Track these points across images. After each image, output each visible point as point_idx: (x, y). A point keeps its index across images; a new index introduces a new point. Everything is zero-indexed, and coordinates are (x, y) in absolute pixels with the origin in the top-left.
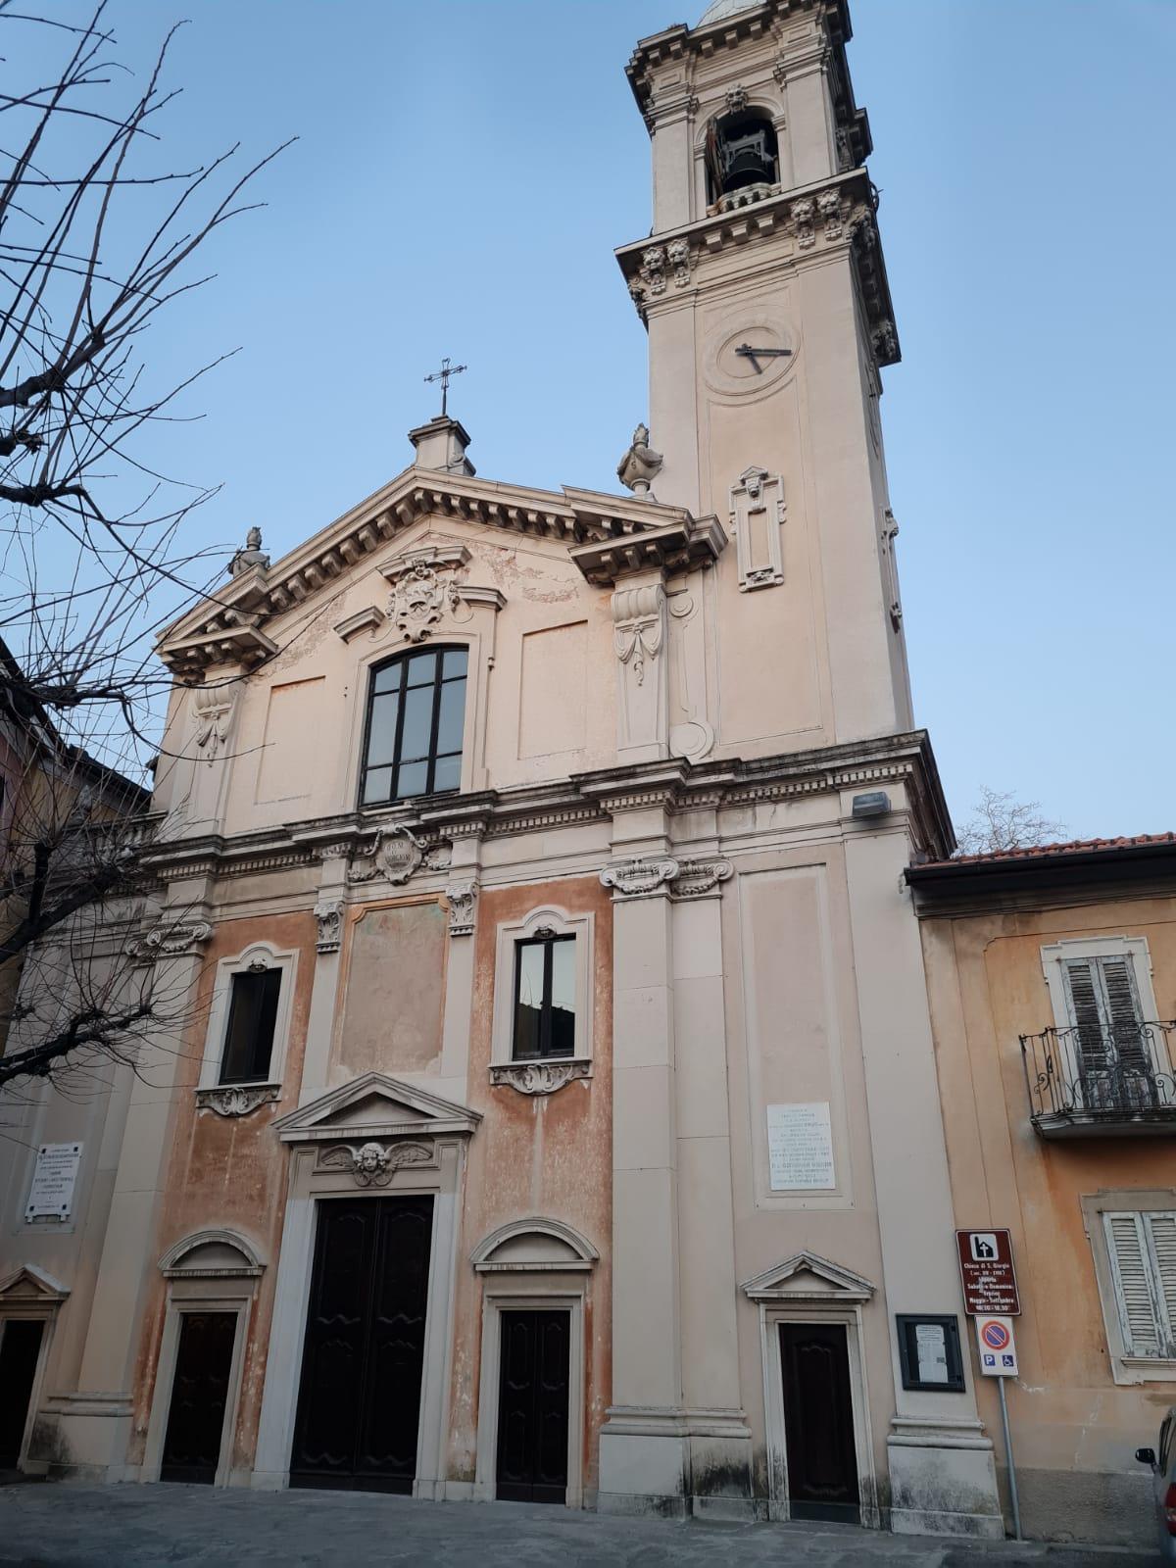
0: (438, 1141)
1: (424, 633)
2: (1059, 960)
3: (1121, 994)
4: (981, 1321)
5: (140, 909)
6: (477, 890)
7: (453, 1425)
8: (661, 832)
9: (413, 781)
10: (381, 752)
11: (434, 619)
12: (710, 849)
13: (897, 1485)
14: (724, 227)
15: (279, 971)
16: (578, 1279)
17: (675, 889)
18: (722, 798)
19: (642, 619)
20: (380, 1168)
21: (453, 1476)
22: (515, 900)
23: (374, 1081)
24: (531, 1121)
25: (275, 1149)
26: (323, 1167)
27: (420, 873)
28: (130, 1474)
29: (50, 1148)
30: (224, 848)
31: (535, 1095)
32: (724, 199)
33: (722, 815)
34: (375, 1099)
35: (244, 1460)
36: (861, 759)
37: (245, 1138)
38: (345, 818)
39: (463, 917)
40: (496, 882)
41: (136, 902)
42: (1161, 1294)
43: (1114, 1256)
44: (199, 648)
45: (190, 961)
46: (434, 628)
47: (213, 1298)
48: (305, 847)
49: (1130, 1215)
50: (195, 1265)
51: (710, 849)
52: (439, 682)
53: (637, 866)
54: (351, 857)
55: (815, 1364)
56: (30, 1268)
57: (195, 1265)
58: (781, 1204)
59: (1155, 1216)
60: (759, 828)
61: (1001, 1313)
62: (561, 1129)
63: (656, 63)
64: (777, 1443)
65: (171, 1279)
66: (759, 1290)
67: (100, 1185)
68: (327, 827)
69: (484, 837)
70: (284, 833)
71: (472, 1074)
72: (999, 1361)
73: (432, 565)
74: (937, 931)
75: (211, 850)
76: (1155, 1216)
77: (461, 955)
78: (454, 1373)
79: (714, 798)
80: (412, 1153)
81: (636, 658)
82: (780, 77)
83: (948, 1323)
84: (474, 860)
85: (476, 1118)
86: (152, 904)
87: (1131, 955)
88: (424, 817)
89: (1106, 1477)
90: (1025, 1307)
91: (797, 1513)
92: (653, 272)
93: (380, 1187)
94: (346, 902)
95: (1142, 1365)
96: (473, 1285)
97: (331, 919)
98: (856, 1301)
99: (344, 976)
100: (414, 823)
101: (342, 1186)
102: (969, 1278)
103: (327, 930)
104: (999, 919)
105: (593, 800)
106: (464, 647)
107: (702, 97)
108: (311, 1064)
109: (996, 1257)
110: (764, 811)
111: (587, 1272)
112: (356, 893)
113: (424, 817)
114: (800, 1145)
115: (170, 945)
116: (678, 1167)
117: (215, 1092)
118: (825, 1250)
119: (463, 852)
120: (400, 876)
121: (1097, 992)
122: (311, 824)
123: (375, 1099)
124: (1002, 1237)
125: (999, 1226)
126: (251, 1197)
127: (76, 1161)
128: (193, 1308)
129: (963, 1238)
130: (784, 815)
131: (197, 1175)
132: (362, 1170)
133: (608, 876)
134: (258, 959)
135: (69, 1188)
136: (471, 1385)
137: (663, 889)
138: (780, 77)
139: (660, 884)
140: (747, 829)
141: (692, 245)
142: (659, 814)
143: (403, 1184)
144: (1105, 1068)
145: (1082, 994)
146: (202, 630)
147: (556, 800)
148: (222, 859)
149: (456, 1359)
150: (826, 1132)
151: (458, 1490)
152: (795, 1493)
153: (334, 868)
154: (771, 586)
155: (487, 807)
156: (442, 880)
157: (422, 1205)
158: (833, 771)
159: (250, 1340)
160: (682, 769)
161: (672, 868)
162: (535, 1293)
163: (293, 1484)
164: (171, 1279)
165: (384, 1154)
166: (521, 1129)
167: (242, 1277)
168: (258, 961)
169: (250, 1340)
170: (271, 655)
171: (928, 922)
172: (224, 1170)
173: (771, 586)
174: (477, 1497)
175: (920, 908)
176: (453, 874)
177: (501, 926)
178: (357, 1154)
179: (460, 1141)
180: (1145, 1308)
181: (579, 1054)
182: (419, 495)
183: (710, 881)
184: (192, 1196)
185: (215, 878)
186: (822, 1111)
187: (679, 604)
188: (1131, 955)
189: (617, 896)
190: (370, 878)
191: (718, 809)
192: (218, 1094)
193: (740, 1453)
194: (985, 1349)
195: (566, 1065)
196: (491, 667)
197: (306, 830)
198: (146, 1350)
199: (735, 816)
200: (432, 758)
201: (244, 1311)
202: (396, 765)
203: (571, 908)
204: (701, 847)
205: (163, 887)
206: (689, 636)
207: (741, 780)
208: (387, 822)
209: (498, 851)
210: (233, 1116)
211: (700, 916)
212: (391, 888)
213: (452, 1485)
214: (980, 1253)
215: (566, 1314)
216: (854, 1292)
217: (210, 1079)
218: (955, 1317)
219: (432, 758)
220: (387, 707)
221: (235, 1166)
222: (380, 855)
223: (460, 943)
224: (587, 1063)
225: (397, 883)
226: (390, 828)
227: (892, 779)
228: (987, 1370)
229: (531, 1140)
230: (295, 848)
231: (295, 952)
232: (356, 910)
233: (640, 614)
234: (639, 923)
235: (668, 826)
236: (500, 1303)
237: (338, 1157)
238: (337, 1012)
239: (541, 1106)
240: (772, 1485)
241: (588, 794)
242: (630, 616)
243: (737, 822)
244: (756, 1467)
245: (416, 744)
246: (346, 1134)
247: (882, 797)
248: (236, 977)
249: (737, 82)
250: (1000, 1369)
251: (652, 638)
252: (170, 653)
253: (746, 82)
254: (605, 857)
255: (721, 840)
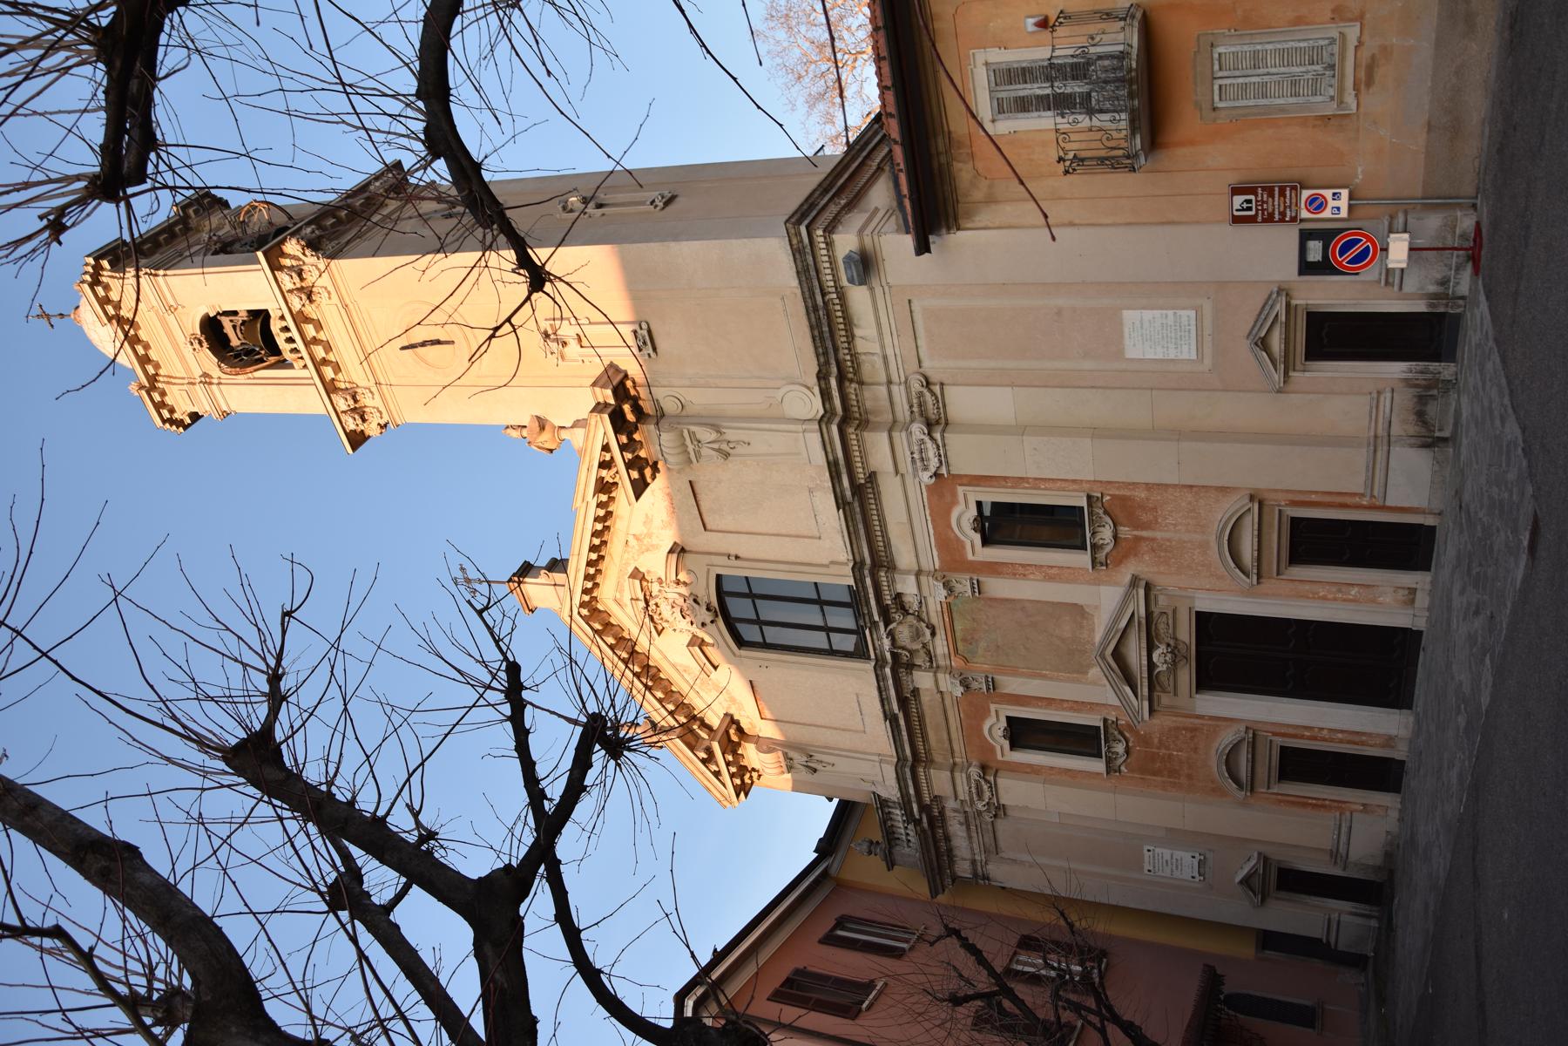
0: (1153, 608)
1: (708, 609)
2: (993, 121)
3: (1023, 74)
4: (1305, 214)
5: (955, 811)
6: (939, 575)
7: (1373, 601)
8: (885, 435)
9: (844, 619)
10: (818, 639)
11: (695, 601)
12: (899, 393)
13: (1432, 288)
14: (319, 365)
15: (1008, 718)
16: (1266, 509)
17: (935, 423)
18: (851, 381)
19: (688, 441)
20: (1174, 651)
21: (1412, 601)
22: (948, 545)
23: (1102, 656)
24: (1138, 539)
25: (1156, 721)
26: (1171, 689)
27: (924, 616)
28: (1394, 815)
29: (1147, 867)
30: (906, 759)
31: (1115, 537)
32: (288, 356)
33: (866, 378)
34: (1118, 655)
35: (1389, 741)
36: (813, 273)
37: (1145, 740)
38: (880, 678)
39: (963, 586)
40: (931, 559)
41: (949, 813)
42: (1283, 70)
43: (1252, 103)
44: (732, 776)
45: (1000, 781)
46: (703, 600)
47: (1268, 761)
48: (903, 702)
49: (1216, 88)
50: (1243, 772)
51: (899, 393)
52: (751, 595)
53: (916, 456)
54: (911, 666)
55: (1335, 337)
56: (1238, 878)
57: (1243, 772)
58: (1208, 351)
59: (1216, 67)
60: (878, 351)
61: (1298, 197)
62: (1145, 517)
63: (172, 411)
64: (1396, 370)
65: (1252, 790)
66: (1277, 377)
67: (1174, 837)
68: (887, 689)
69: (891, 567)
70: (890, 718)
71: (1097, 582)
72: (1336, 203)
73: (647, 602)
74: (969, 215)
75: (908, 770)
76: (1216, 67)
77: (998, 587)
78: (1335, 599)
79: (852, 388)
80: (1162, 627)
81: (724, 447)
82: (171, 309)
83: (1306, 236)
84: (912, 578)
85: (1135, 582)
86: (950, 804)
87: (987, 64)
88: (876, 618)
89: (1430, 127)
90: (1295, 173)
91: (1451, 357)
92: (364, 420)
93: (1188, 648)
94: (950, 671)
95: (1341, 90)
96: (1267, 585)
97: (965, 684)
98: (1288, 305)
99: (1014, 672)
100: (882, 625)
101: (1186, 676)
102: (1269, 219)
103: (975, 685)
104: (956, 165)
105: (857, 489)
106: (719, 577)
107: (197, 372)
108: (1090, 695)
109: (1252, 197)
110: (861, 346)
111: (1261, 504)
112: (942, 663)
113: (876, 618)
114: (1157, 335)
115: (987, 794)
116: (1179, 434)
117: (1108, 763)
118: (1245, 322)
119: (907, 587)
120: (928, 632)
121: (1021, 93)
122: (884, 701)
123: (1118, 655)
124: (1236, 191)
125: (1228, 190)
126: (1192, 738)
127: (1158, 850)
128: (1275, 773)
129: (1236, 220)
130: (865, 333)
131: (1173, 773)
132: (1174, 663)
133: (926, 477)
134: (999, 732)
135: (1178, 854)
136: (1344, 589)
137: (937, 436)
138: (171, 309)
139: (932, 438)
140: (879, 362)
141: (336, 390)
142: (868, 436)
143: (1186, 633)
144: (1089, 94)
145: (1023, 105)
146: (717, 774)
147: (861, 526)
148: (913, 758)
149: (1324, 598)
150: (1148, 315)
151: (1422, 600)
152: (1437, 358)
153: (923, 680)
154: (649, 332)
155: (866, 572)
156: (930, 601)
157: (1203, 619)
158: (824, 294)
159: (1302, 737)
160: (829, 422)
161: (918, 429)
162: (1276, 541)
163: (1410, 707)
164: (1252, 790)
165: (1162, 648)
166: (1144, 547)
167: (1253, 745)
168: (1000, 733)
169: (1302, 737)
170: (732, 721)
171: (962, 223)
172: (1170, 756)
173: (649, 332)
174: (1428, 587)
175: (949, 229)
176: (925, 592)
177: (970, 557)
178: (1162, 668)
179: (1153, 593)
180: (1294, 83)
181: (1083, 503)
182: (585, 612)
183: (928, 395)
184: (1189, 777)
185: (930, 762)
186: (1130, 316)
187: (670, 406)
188: (987, 64)
189: (944, 471)
190: (928, 653)
191: (861, 383)
192: (1109, 762)
193: (1405, 398)
194: (1327, 214)
195: (1091, 513)
196: (737, 557)
197: (890, 703)
198: (1305, 805)
199: (866, 371)
200: (820, 602)
201: (1279, 741)
202: (828, 630)
203: (954, 502)
204: (897, 399)
205: (937, 799)
206: (699, 399)
207: (834, 370)
208: (882, 646)
209: (904, 556)
210: (1127, 751)
211: (962, 402)
212: (938, 637)
213: (1418, 603)
214: (1249, 209)
215: (1293, 519)
216: (1280, 307)
217: (1098, 766)
218: (1301, 231)
219: (820, 602)
220: (773, 634)
221: (1167, 748)
222: (909, 647)
223: (985, 588)
224: (1089, 497)
225: (933, 634)
226: (887, 643)
227: (829, 245)
228: (1344, 213)
229: (1153, 539)
230: (904, 713)
231: (993, 707)
232: (957, 663)
233: (684, 444)
234: (966, 455)
235: (877, 427)
236: (1283, 565)
237: (1163, 679)
238: (1044, 677)
239: (1125, 531)
240: (1429, 376)
241: (853, 495)
242: (686, 452)
243: (872, 368)
244: (1416, 386)
245: (812, 615)
246: (1145, 675)
247: (848, 259)
248: (1013, 747)
249: (182, 346)
250: (1343, 203)
251: (706, 435)
252: (738, 796)
253: (181, 339)
254: (909, 480)
255: (890, 382)
